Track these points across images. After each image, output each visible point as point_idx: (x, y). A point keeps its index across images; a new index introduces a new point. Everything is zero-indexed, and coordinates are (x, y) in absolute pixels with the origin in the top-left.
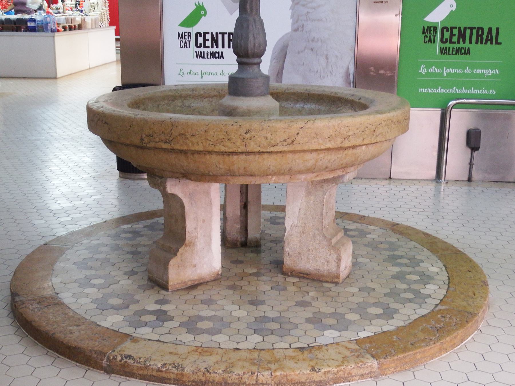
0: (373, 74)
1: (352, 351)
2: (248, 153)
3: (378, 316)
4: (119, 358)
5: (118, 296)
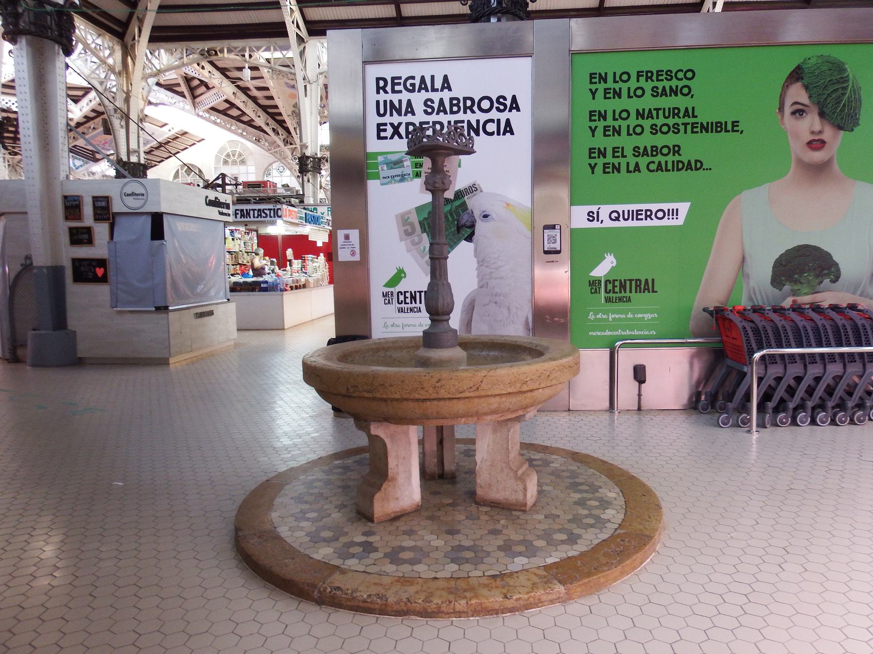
0: (549, 320)
1: (541, 577)
2: (439, 399)
3: (563, 542)
4: (329, 590)
5: (329, 529)
